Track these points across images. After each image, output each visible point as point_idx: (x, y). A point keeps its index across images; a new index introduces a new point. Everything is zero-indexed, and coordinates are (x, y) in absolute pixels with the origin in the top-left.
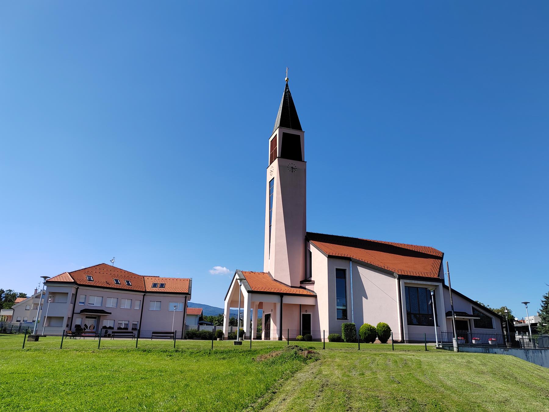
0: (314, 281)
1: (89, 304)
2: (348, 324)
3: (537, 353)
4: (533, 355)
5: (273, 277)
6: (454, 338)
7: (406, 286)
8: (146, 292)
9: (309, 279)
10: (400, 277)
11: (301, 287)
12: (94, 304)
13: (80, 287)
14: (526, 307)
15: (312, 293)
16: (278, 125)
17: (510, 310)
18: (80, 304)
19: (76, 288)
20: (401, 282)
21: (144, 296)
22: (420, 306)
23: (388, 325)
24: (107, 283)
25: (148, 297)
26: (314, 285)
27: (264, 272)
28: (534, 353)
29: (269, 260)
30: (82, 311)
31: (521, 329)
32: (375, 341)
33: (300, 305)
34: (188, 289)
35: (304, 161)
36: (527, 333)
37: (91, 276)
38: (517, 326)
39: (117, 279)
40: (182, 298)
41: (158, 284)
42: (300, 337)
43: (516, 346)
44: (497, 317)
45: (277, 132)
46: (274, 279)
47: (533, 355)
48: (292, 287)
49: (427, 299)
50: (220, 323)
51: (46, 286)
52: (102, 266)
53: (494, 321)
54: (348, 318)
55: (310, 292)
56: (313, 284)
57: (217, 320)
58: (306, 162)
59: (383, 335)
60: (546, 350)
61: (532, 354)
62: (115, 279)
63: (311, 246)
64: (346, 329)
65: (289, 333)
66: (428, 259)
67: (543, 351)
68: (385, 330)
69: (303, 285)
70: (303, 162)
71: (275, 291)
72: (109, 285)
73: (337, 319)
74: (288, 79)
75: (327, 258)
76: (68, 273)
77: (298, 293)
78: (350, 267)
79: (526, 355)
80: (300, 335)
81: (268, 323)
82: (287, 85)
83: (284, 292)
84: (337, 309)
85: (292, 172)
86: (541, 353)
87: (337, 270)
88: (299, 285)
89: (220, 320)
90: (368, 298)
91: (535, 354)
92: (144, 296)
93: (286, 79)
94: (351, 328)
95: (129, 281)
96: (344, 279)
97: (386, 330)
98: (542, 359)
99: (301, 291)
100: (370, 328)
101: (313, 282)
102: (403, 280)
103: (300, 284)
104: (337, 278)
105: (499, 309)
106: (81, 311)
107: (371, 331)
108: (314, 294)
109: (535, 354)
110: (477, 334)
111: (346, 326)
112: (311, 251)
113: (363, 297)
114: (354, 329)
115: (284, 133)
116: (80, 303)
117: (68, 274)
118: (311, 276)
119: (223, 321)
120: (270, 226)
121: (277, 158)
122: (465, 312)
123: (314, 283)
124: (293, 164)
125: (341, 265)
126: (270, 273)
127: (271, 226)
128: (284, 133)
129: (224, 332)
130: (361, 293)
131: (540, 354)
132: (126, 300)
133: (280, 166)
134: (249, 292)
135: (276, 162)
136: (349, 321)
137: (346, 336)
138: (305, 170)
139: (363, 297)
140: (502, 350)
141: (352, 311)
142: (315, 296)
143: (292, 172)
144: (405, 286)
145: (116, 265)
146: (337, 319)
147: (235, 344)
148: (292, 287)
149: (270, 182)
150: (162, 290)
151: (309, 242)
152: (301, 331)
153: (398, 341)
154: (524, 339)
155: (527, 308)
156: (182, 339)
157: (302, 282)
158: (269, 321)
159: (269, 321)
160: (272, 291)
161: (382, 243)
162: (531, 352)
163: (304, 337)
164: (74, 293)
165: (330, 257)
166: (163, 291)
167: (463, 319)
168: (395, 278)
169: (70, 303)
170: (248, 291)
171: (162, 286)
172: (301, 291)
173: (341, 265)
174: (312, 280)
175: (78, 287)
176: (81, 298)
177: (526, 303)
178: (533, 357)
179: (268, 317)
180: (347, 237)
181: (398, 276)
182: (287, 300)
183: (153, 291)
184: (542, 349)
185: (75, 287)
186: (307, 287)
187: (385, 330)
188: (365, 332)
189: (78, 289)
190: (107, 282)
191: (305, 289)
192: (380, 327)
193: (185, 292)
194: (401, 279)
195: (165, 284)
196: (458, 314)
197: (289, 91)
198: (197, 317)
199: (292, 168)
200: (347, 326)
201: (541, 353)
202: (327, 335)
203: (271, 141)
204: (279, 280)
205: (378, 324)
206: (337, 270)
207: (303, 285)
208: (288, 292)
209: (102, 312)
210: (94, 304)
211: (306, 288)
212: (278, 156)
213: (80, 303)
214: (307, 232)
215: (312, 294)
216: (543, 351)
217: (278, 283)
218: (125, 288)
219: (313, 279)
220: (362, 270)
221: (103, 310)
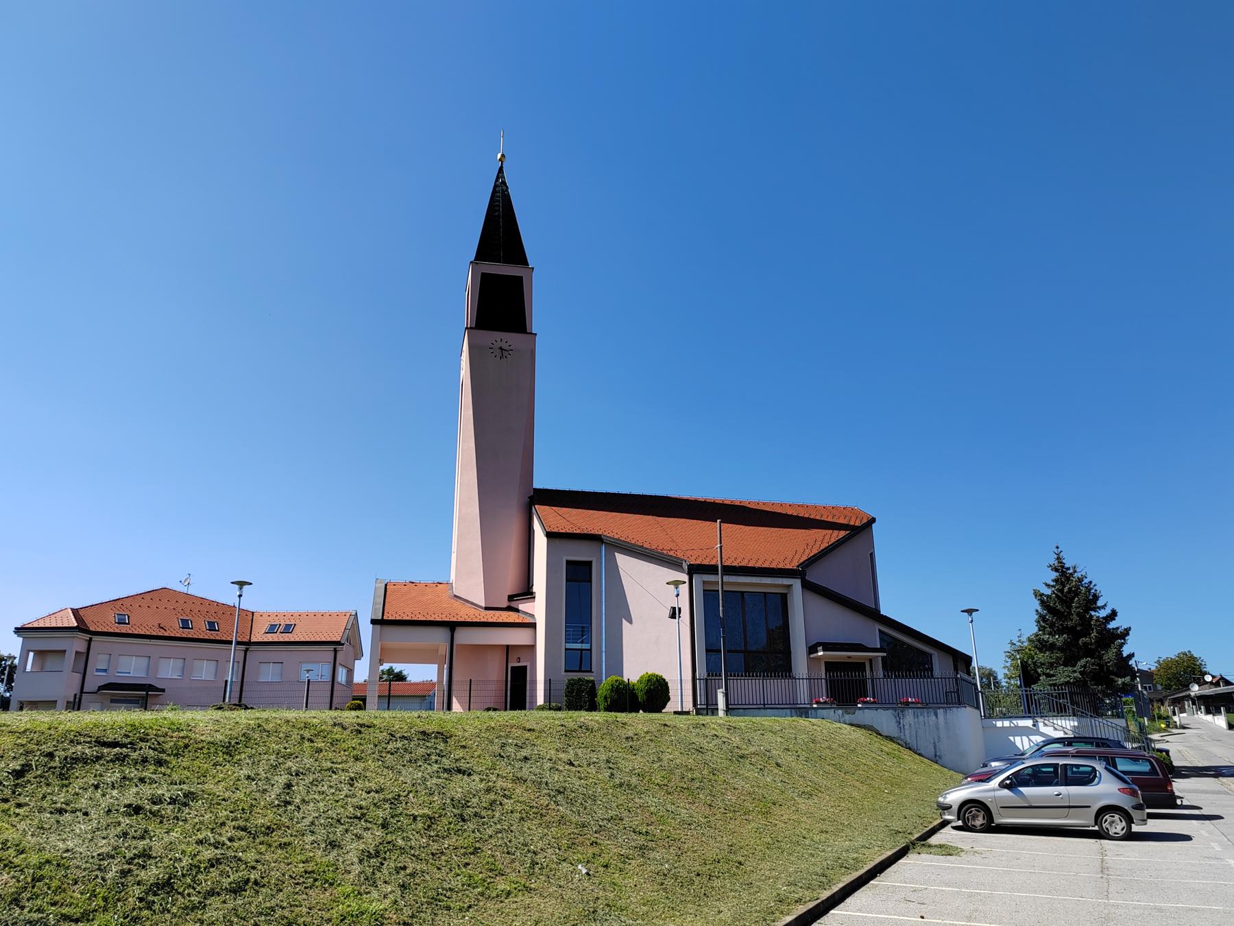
1: (118, 672)
2: (574, 680)
3: (926, 715)
4: (916, 720)
6: (721, 690)
7: (706, 589)
8: (250, 643)
10: (693, 570)
11: (509, 609)
12: (129, 673)
13: (95, 638)
14: (970, 619)
17: (1200, 658)
18: (98, 674)
19: (86, 640)
21: (246, 651)
22: (748, 634)
23: (664, 677)
24: (162, 628)
25: (255, 656)
26: (534, 601)
28: (918, 716)
30: (101, 688)
31: (1210, 700)
33: (508, 646)
35: (531, 333)
36: (1222, 708)
37: (125, 615)
38: (1202, 694)
39: (212, 621)
41: (280, 625)
43: (850, 702)
44: (942, 650)
46: (455, 596)
47: (916, 720)
48: (487, 608)
49: (766, 618)
51: (22, 639)
52: (161, 594)
53: (937, 662)
56: (532, 600)
58: (536, 334)
59: (647, 700)
60: (948, 710)
61: (912, 718)
62: (182, 618)
64: (569, 692)
65: (468, 704)
66: (811, 531)
67: (942, 710)
68: (650, 688)
69: (514, 604)
70: (529, 335)
72: (165, 630)
73: (566, 671)
74: (503, 155)
76: (70, 610)
77: (494, 620)
78: (601, 556)
79: (897, 722)
82: (501, 170)
84: (566, 649)
86: (936, 715)
87: (568, 562)
88: (505, 604)
90: (633, 620)
91: (921, 718)
92: (246, 651)
93: (499, 156)
94: (580, 688)
95: (214, 622)
97: (654, 688)
98: (938, 729)
102: (699, 575)
104: (567, 580)
105: (1173, 657)
106: (99, 687)
109: (921, 718)
110: (818, 679)
113: (624, 621)
115: (483, 274)
116: (98, 670)
117: (71, 612)
122: (861, 644)
123: (534, 597)
124: (504, 341)
125: (580, 553)
128: (483, 274)
130: (621, 611)
131: (934, 718)
132: (205, 661)
136: (593, 674)
139: (624, 621)
140: (840, 712)
144: (704, 590)
145: (196, 590)
146: (566, 671)
148: (487, 608)
152: (509, 701)
154: (954, 692)
155: (678, 595)
157: (511, 598)
161: (717, 501)
162: (911, 715)
164: (83, 649)
167: (849, 657)
169: (71, 670)
171: (288, 629)
173: (580, 553)
175: (91, 639)
176: (99, 660)
177: (970, 612)
178: (915, 725)
180: (570, 491)
182: (465, 637)
183: (266, 640)
184: (939, 708)
185: (83, 639)
186: (522, 607)
187: (650, 688)
189: (92, 643)
190: (161, 626)
191: (517, 610)
193: (335, 639)
195: (295, 625)
196: (827, 647)
197: (504, 183)
199: (501, 348)
200: (573, 685)
201: (936, 715)
204: (463, 597)
206: (568, 562)
207: (514, 604)
209: (150, 687)
210: (129, 673)
213: (98, 670)
214: (535, 489)
216: (940, 712)
218: (201, 637)
220: (622, 560)
221: (150, 686)
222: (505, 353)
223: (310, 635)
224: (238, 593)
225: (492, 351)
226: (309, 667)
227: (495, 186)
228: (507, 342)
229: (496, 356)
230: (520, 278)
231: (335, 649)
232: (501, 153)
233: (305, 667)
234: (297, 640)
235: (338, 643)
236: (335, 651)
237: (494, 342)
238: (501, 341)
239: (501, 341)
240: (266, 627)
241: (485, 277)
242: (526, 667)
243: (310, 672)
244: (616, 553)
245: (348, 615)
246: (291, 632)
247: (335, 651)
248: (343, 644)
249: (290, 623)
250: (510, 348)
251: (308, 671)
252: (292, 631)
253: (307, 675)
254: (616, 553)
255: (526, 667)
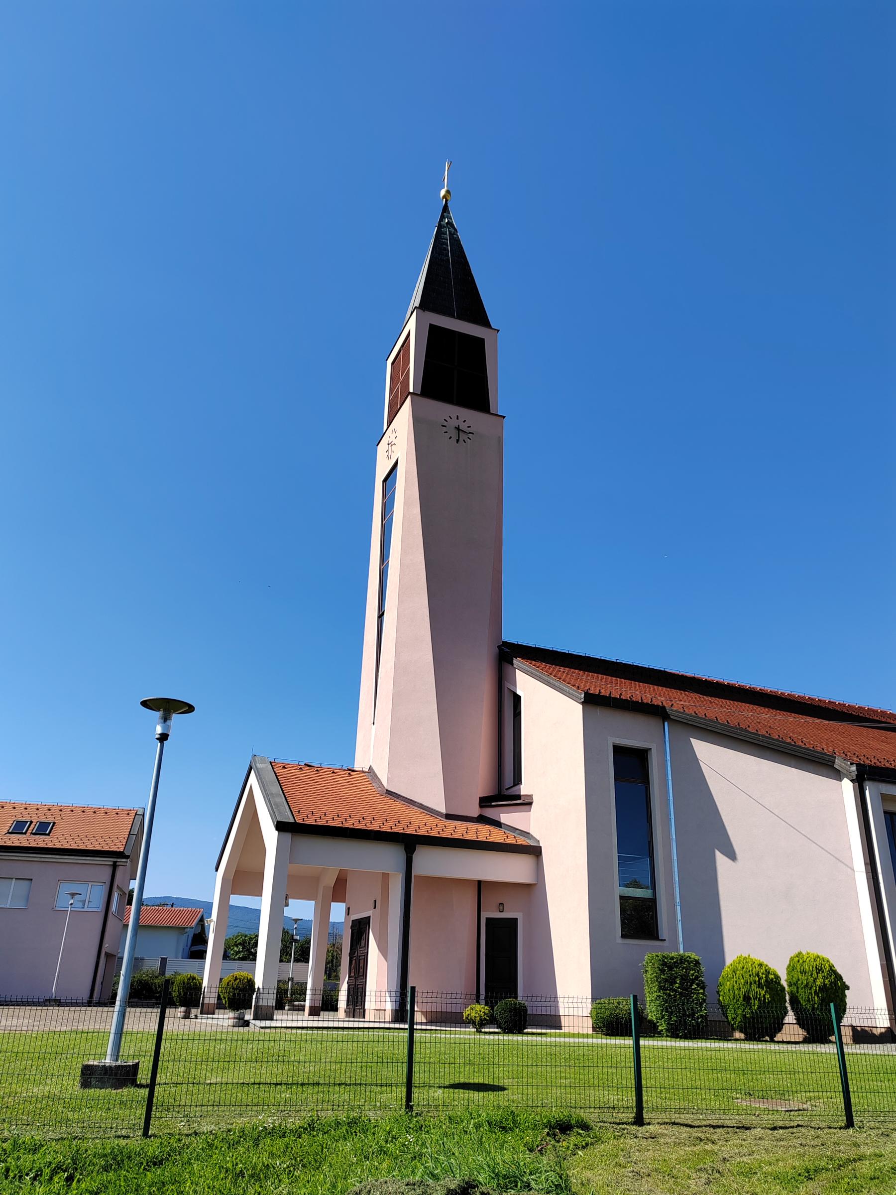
0: (531, 796)
2: (672, 958)
5: (384, 782)
9: (513, 791)
11: (482, 819)
15: (522, 838)
16: (417, 304)
20: (867, 793)
27: (355, 769)
29: (374, 727)
32: (780, 1030)
34: (124, 843)
40: (101, 870)
41: (31, 822)
42: (479, 1010)
45: (411, 326)
46: (389, 792)
48: (449, 817)
50: (248, 950)
54: (664, 930)
55: (517, 836)
56: (527, 807)
57: (240, 944)
63: (519, 675)
64: (666, 980)
69: (490, 813)
70: (491, 416)
71: (386, 829)
74: (448, 192)
75: (583, 703)
77: (471, 836)
80: (478, 1002)
81: (360, 951)
82: (445, 209)
83: (422, 832)
85: (458, 441)
87: (618, 750)
88: (475, 811)
89: (249, 943)
93: (443, 192)
94: (687, 975)
96: (85, 995)
97: (831, 983)
99: (484, 833)
100: (767, 977)
101: (526, 801)
103: (481, 806)
104: (616, 779)
107: (771, 989)
108: (532, 843)
111: (664, 964)
112: (519, 692)
113: (718, 853)
114: (697, 977)
118: (518, 780)
119: (881, 964)
120: (381, 616)
121: (409, 397)
123: (530, 804)
124: (461, 420)
126: (374, 772)
127: (383, 614)
129: (259, 983)
133: (418, 421)
134: (281, 827)
135: (406, 410)
136: (666, 944)
137: (667, 1007)
138: (500, 441)
139: (718, 853)
141: (674, 905)
142: (535, 852)
143: (458, 441)
144: (885, 812)
147: (85, 1084)
148: (449, 817)
149: (385, 481)
150: (40, 841)
151: (512, 664)
153: (874, 1031)
156: (89, 1004)
157: (485, 802)
158: (363, 942)
159: (363, 944)
160: (375, 827)
163: (493, 1009)
165: (591, 701)
166: (42, 845)
168: (838, 775)
170: (278, 822)
171: (44, 829)
172: (484, 833)
174: (522, 793)
179: (360, 929)
181: (854, 768)
183: (9, 843)
188: (748, 992)
191: (498, 824)
192: (803, 972)
193: (114, 849)
194: (869, 779)
195: (54, 823)
197: (450, 224)
198: (183, 934)
199: (458, 429)
202: (585, 1007)
203: (393, 363)
205: (792, 959)
206: (618, 750)
207: (490, 813)
208: (434, 834)
211: (502, 821)
212: (411, 390)
215: (522, 841)
217: (398, 805)
219: (524, 789)
222: (463, 436)
223: (78, 840)
224: (159, 730)
225: (445, 429)
226: (74, 888)
227: (440, 226)
228: (465, 421)
229: (450, 438)
230: (482, 341)
231: (115, 862)
232: (446, 188)
233: (66, 888)
234: (58, 846)
235: (120, 855)
236: (115, 866)
237: (448, 419)
238: (458, 418)
239: (458, 418)
240: (9, 824)
241: (433, 328)
242: (515, 921)
243: (77, 897)
244: (691, 739)
245: (133, 814)
246: (48, 834)
247: (115, 866)
248: (128, 857)
249: (23, 820)
250: (469, 430)
251: (73, 895)
252: (50, 832)
253: (72, 901)
254: (691, 739)
255: (515, 921)
